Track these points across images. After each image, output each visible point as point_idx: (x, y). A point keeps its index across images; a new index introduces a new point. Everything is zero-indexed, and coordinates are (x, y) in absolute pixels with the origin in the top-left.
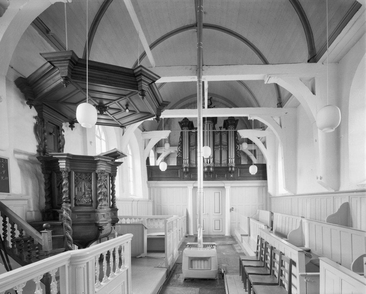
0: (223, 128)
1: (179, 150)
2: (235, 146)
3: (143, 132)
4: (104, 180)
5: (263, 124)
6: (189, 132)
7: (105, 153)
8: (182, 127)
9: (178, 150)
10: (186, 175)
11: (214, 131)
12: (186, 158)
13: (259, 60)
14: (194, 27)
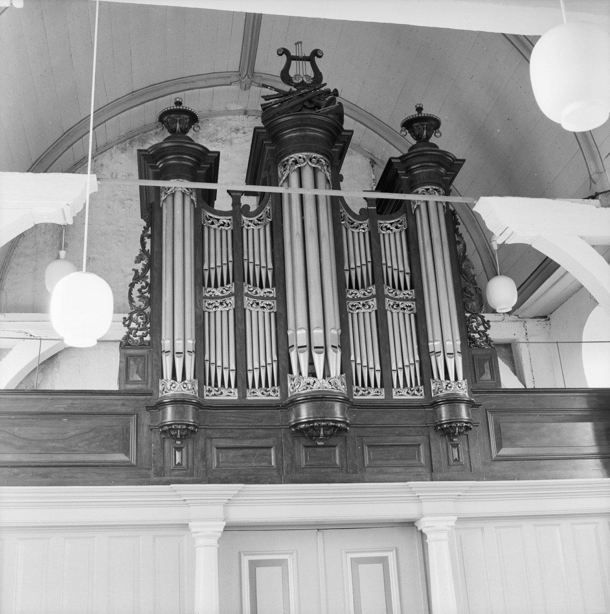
1: (138, 303)
9: (131, 300)
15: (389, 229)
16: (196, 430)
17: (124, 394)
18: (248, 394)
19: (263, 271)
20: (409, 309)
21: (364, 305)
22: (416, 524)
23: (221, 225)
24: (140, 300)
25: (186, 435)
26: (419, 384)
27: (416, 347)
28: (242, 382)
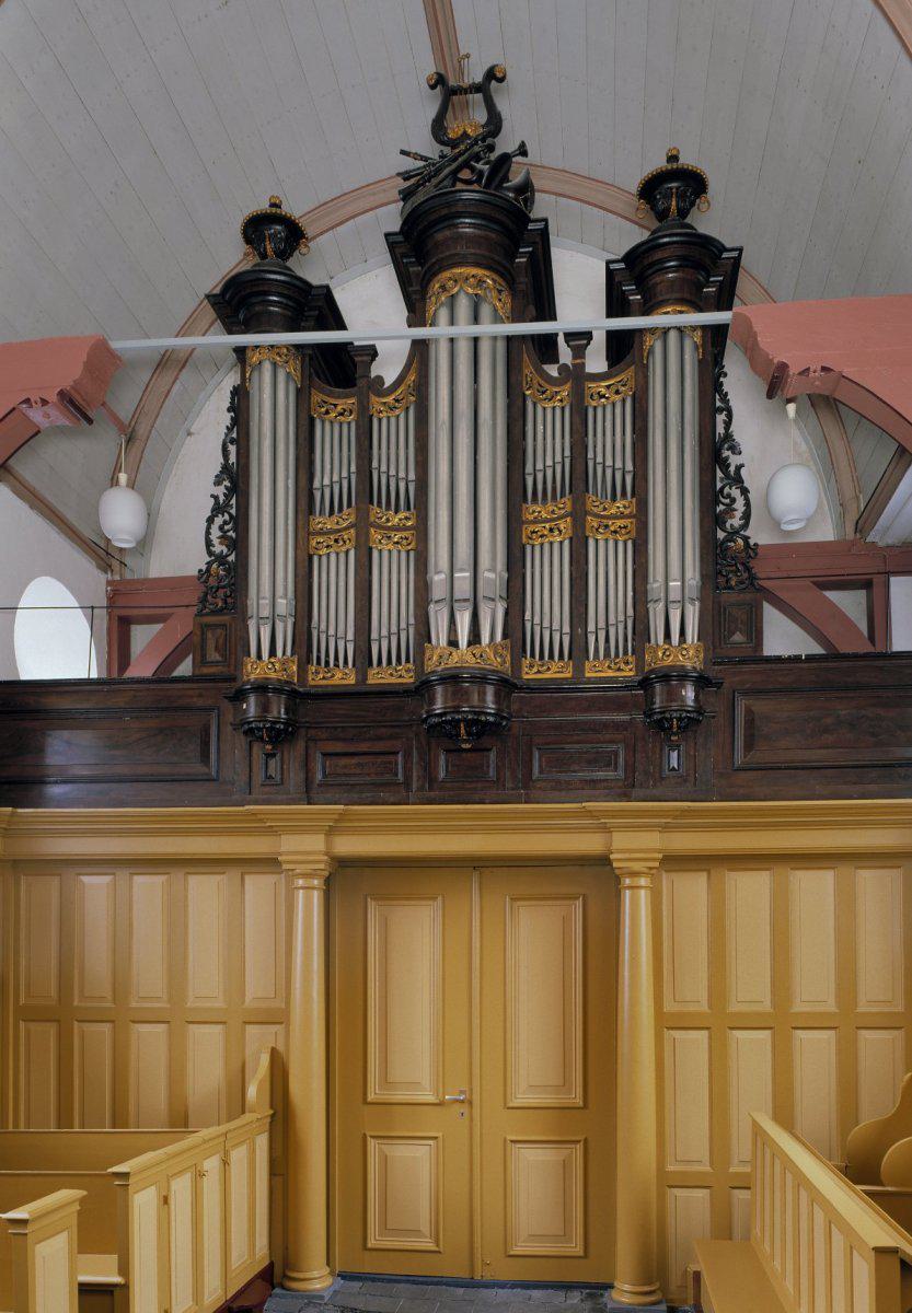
1: (218, 548)
9: (209, 543)
15: (603, 396)
16: (504, 723)
17: (198, 681)
18: (370, 677)
19: (402, 485)
20: (623, 531)
21: (336, 541)
22: (337, 864)
23: (341, 414)
24: (221, 543)
25: (687, 726)
26: (602, 657)
27: (630, 594)
28: (364, 658)
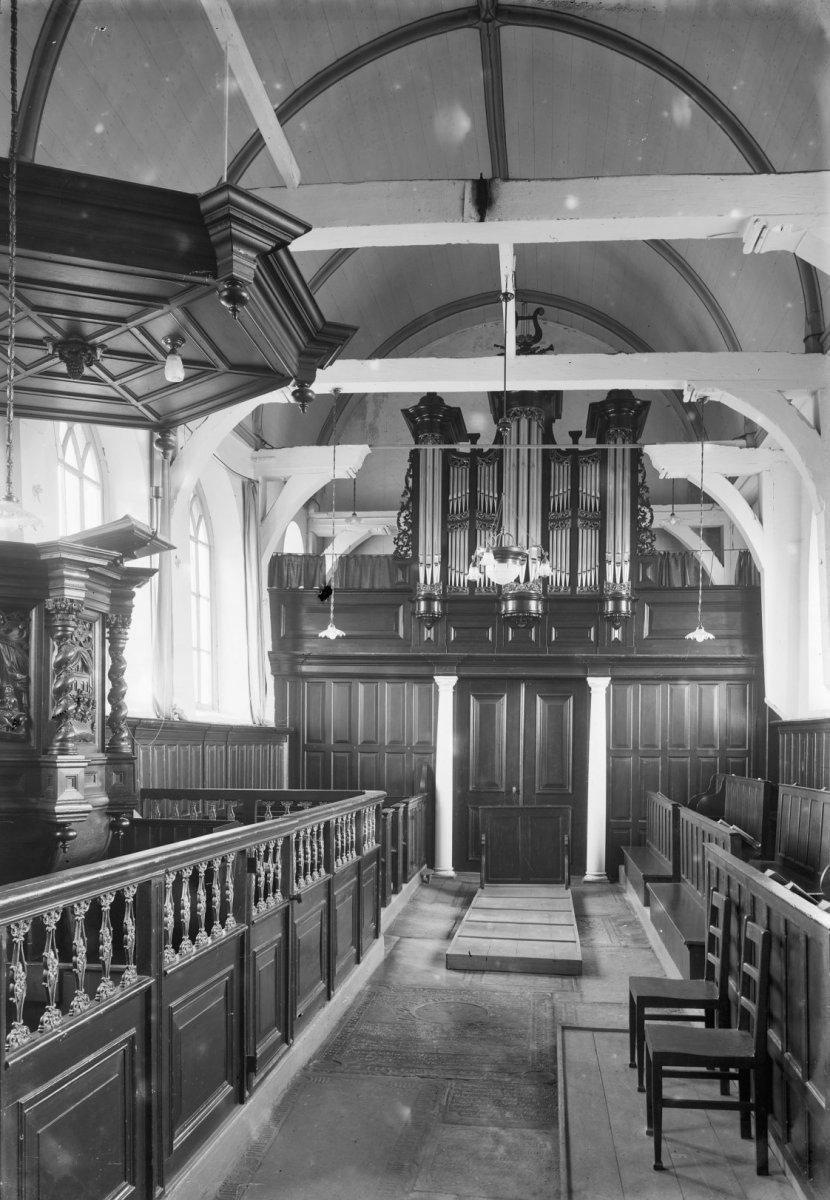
0: (587, 436)
1: (403, 527)
2: (635, 512)
3: (257, 450)
4: (82, 640)
5: (748, 422)
6: (446, 454)
7: (99, 528)
8: (417, 432)
9: (399, 525)
10: (429, 628)
11: (547, 447)
12: (429, 559)
13: (736, 156)
14: (469, 22)
